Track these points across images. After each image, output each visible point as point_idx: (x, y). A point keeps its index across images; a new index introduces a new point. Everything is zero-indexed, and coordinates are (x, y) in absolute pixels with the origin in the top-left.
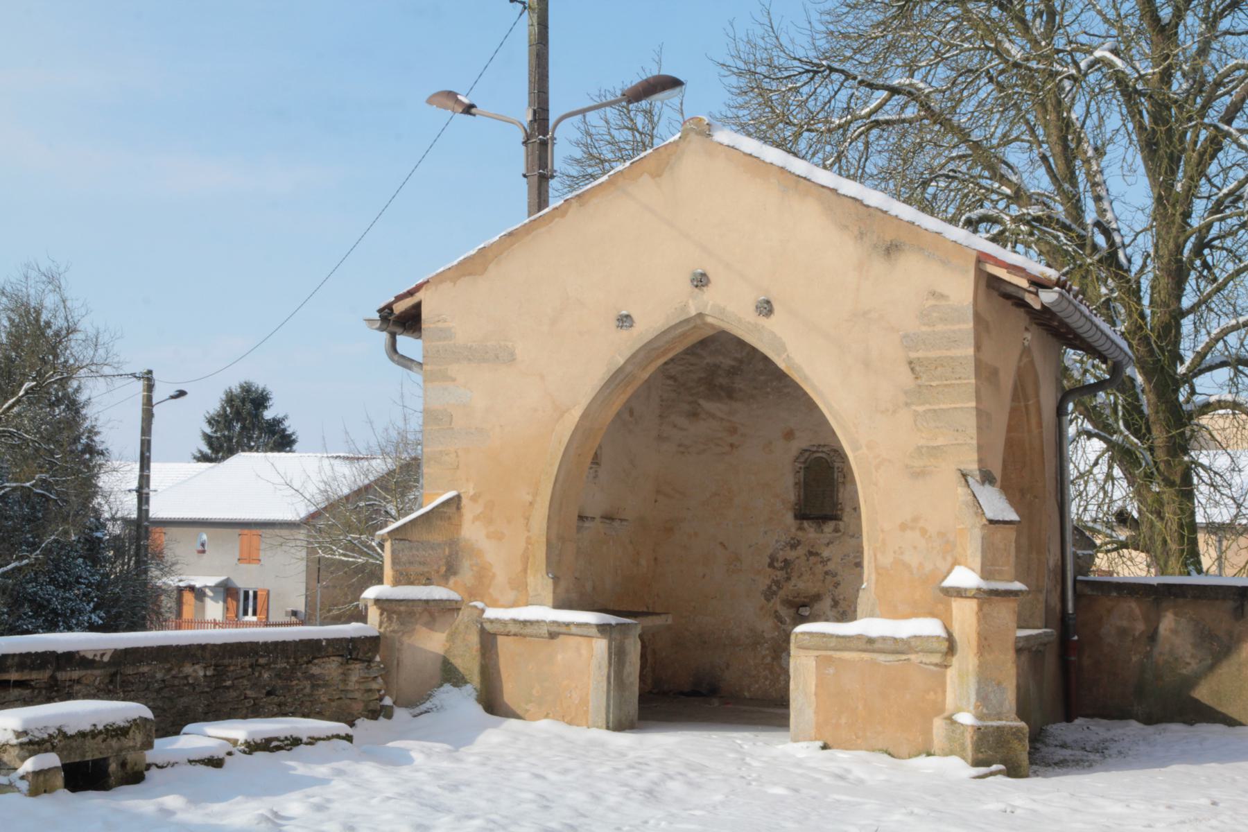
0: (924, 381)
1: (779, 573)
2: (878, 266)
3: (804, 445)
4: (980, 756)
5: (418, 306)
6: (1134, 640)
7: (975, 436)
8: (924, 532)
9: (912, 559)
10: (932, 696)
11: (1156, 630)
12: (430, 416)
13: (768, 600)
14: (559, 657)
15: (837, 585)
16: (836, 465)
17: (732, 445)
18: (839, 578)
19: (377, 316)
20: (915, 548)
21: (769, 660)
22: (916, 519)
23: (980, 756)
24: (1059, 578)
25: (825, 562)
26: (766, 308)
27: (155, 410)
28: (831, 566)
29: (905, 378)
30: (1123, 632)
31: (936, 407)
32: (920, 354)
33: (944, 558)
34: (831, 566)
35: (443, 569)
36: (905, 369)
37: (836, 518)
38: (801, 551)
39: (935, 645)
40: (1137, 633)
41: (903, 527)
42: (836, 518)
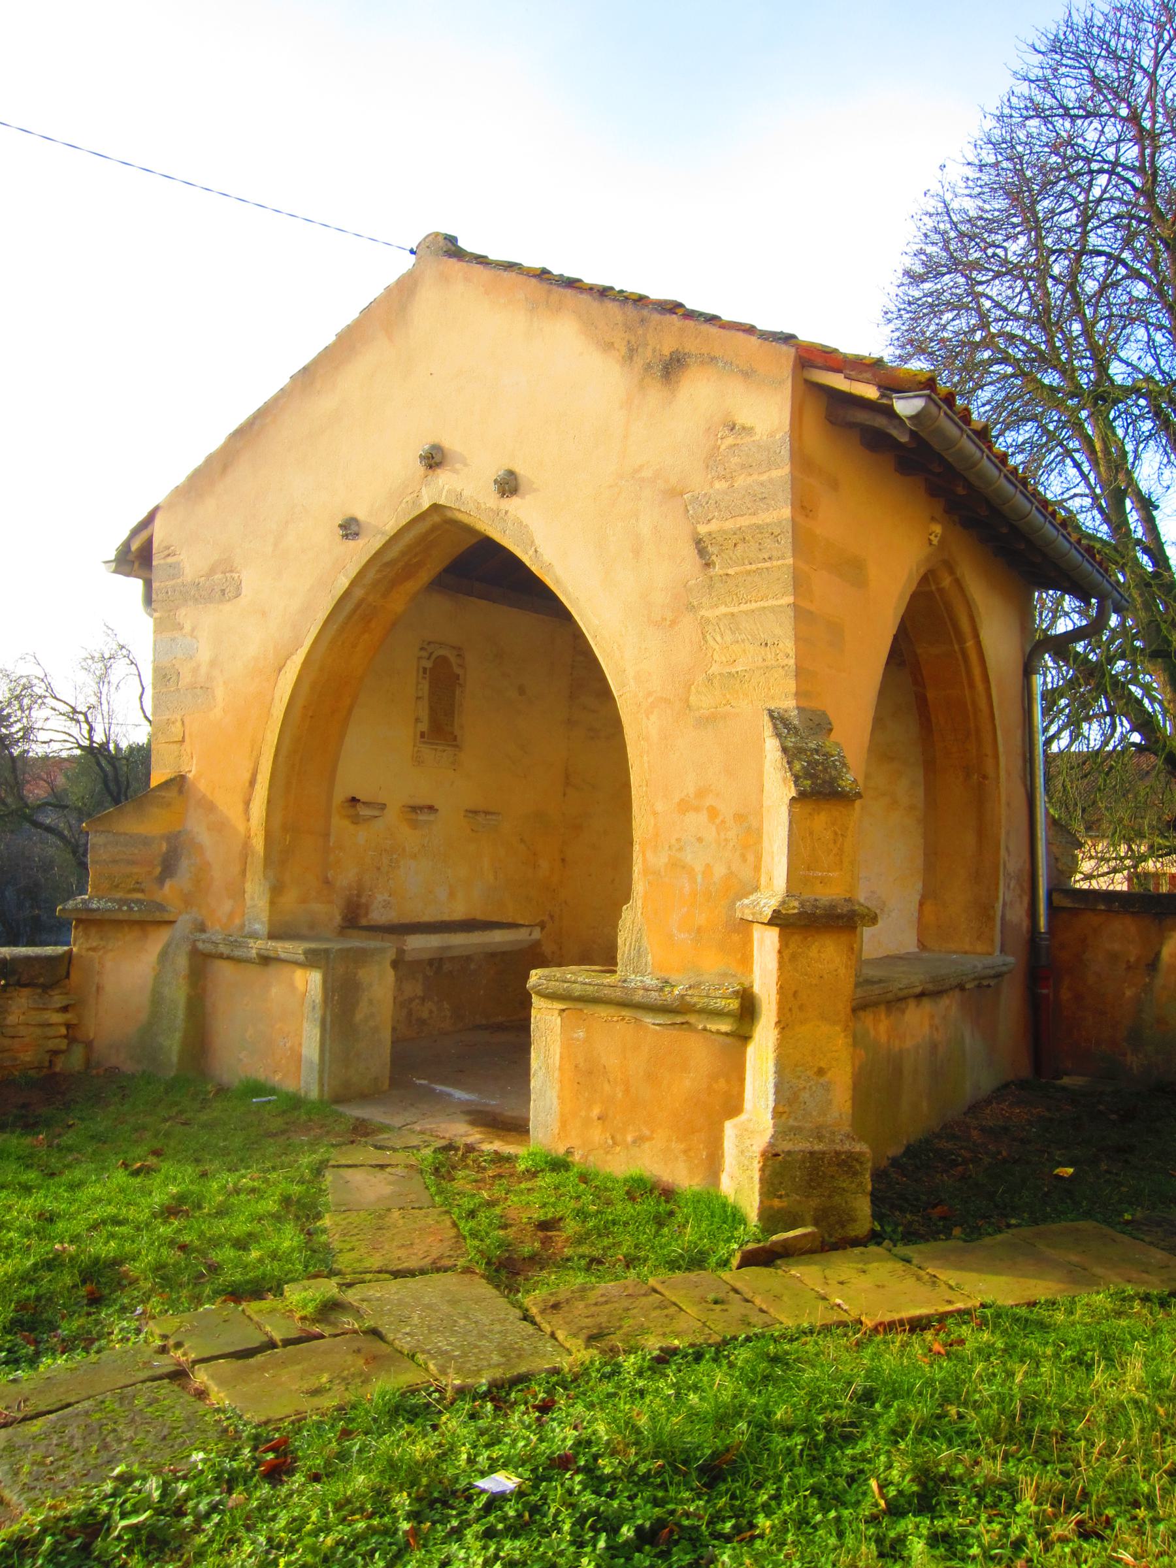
0: (717, 570)
2: (655, 394)
4: (777, 1203)
6: (1129, 968)
7: (792, 654)
8: (713, 813)
11: (1158, 954)
14: (274, 990)
22: (701, 793)
23: (777, 1203)
24: (1026, 885)
26: (509, 485)
30: (1114, 957)
31: (735, 610)
32: (714, 526)
35: (158, 870)
36: (690, 551)
39: (721, 1004)
40: (1132, 959)
41: (685, 807)
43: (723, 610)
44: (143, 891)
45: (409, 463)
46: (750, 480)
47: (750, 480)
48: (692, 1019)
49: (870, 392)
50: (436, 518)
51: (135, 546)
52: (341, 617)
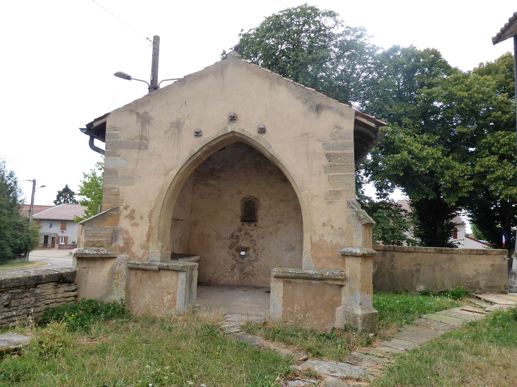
1: (234, 240)
2: (313, 115)
3: (245, 196)
5: (104, 124)
8: (332, 227)
9: (328, 239)
10: (335, 298)
12: (108, 172)
13: (230, 249)
15: (255, 244)
16: (256, 203)
17: (219, 196)
18: (256, 242)
19: (85, 127)
20: (329, 234)
21: (230, 270)
22: (329, 221)
25: (251, 237)
27: (36, 190)
28: (253, 238)
29: (325, 161)
31: (338, 174)
32: (331, 152)
33: (342, 239)
34: (253, 238)
37: (256, 221)
38: (243, 232)
42: (256, 221)
43: (334, 174)
44: (81, 224)
45: (225, 118)
46: (342, 141)
47: (342, 141)
48: (328, 282)
49: (373, 125)
50: (231, 135)
51: (95, 125)
52: (192, 160)
